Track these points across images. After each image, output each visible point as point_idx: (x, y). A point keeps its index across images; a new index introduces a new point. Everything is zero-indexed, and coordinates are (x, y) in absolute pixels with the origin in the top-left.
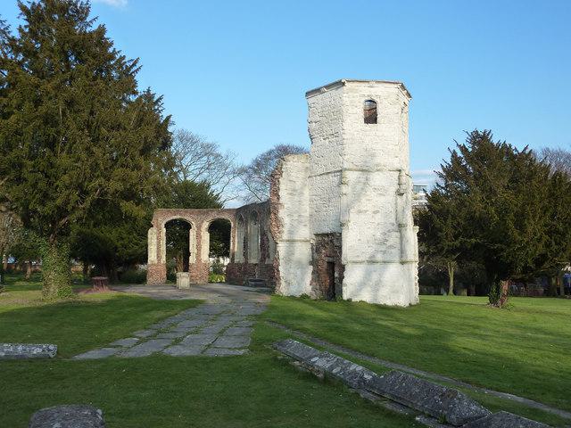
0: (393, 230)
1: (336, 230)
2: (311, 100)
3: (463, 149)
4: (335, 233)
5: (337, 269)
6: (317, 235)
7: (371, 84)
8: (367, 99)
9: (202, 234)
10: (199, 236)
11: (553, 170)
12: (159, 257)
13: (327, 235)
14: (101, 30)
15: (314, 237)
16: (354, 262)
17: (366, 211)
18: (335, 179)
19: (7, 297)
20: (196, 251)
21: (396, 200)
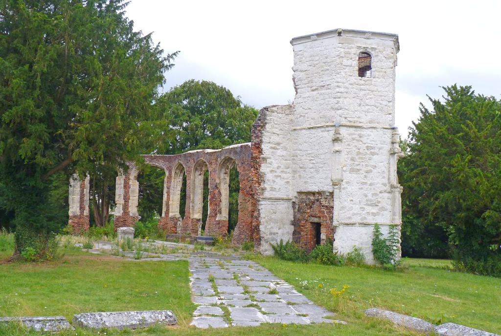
0: (385, 191)
1: (328, 188)
2: (299, 47)
3: (436, 104)
4: (324, 192)
5: (323, 231)
6: (300, 193)
7: (366, 35)
8: (362, 50)
9: (131, 183)
10: (126, 186)
11: (201, 81)
12: (82, 208)
13: (314, 194)
14: (449, 91)
15: (296, 194)
16: (347, 224)
17: (359, 170)
18: (329, 135)
19: (212, 198)
20: (122, 202)
21: (389, 160)
